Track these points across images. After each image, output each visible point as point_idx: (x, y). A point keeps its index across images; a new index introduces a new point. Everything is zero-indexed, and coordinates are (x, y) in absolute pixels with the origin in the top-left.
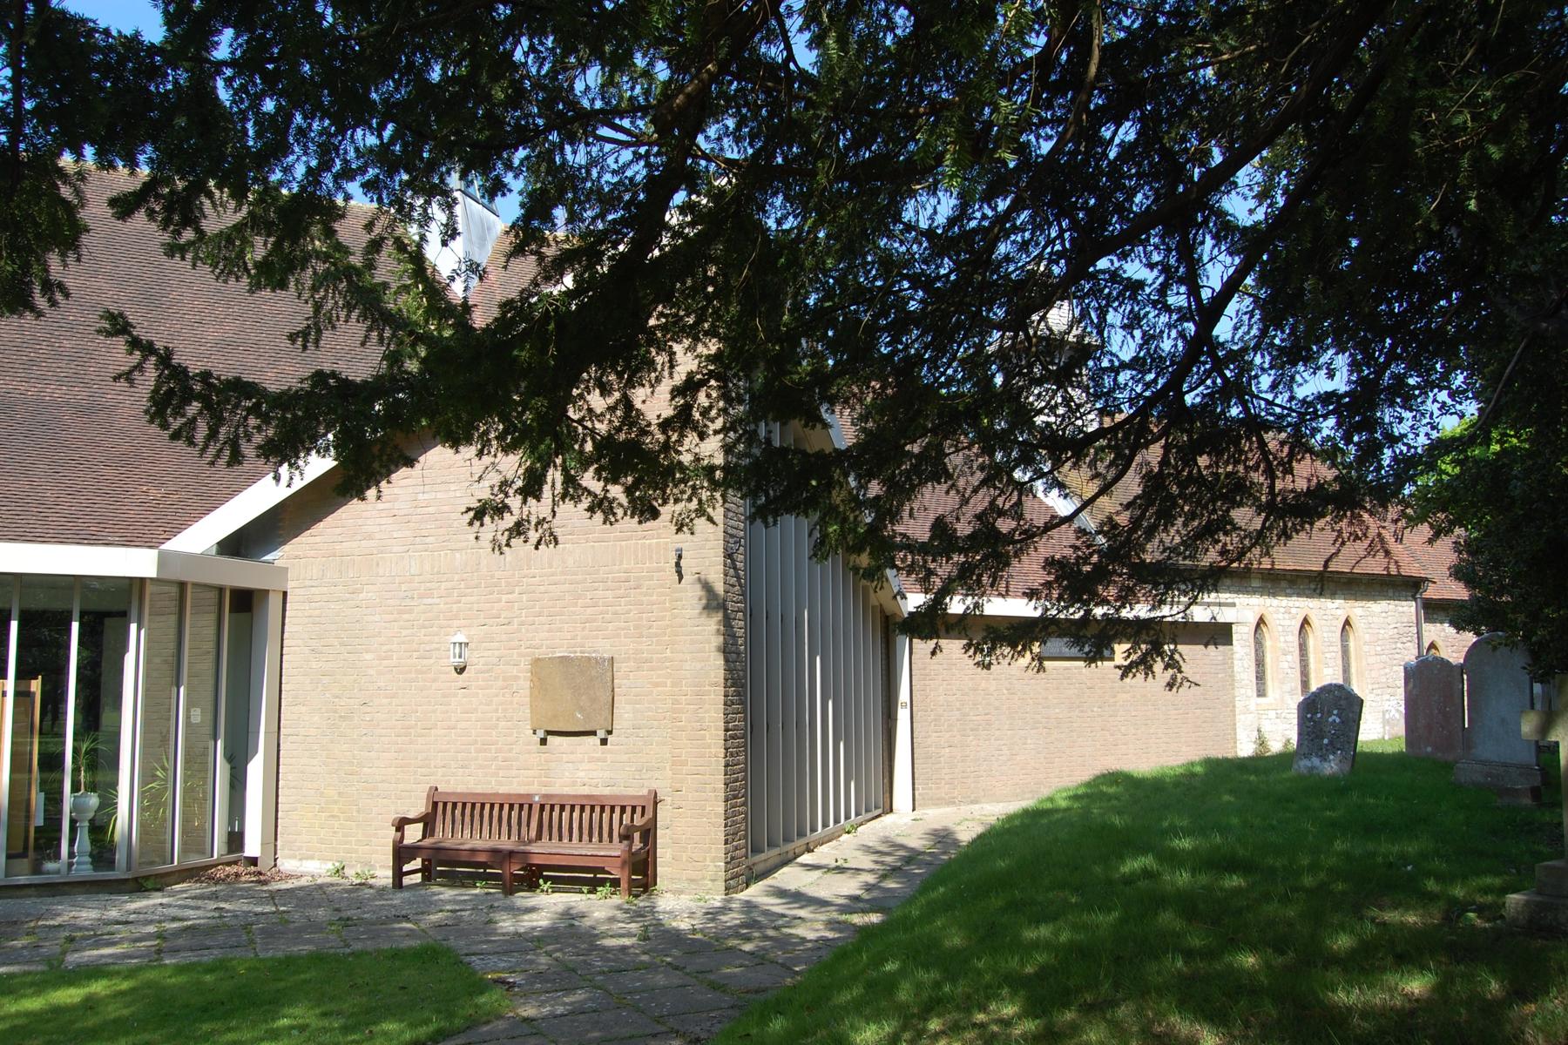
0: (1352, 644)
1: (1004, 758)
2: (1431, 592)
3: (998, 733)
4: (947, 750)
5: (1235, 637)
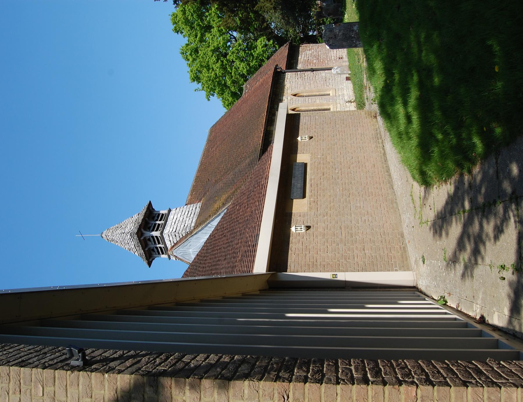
0: (305, 94)
2: (283, 66)
3: (353, 222)
4: (367, 252)
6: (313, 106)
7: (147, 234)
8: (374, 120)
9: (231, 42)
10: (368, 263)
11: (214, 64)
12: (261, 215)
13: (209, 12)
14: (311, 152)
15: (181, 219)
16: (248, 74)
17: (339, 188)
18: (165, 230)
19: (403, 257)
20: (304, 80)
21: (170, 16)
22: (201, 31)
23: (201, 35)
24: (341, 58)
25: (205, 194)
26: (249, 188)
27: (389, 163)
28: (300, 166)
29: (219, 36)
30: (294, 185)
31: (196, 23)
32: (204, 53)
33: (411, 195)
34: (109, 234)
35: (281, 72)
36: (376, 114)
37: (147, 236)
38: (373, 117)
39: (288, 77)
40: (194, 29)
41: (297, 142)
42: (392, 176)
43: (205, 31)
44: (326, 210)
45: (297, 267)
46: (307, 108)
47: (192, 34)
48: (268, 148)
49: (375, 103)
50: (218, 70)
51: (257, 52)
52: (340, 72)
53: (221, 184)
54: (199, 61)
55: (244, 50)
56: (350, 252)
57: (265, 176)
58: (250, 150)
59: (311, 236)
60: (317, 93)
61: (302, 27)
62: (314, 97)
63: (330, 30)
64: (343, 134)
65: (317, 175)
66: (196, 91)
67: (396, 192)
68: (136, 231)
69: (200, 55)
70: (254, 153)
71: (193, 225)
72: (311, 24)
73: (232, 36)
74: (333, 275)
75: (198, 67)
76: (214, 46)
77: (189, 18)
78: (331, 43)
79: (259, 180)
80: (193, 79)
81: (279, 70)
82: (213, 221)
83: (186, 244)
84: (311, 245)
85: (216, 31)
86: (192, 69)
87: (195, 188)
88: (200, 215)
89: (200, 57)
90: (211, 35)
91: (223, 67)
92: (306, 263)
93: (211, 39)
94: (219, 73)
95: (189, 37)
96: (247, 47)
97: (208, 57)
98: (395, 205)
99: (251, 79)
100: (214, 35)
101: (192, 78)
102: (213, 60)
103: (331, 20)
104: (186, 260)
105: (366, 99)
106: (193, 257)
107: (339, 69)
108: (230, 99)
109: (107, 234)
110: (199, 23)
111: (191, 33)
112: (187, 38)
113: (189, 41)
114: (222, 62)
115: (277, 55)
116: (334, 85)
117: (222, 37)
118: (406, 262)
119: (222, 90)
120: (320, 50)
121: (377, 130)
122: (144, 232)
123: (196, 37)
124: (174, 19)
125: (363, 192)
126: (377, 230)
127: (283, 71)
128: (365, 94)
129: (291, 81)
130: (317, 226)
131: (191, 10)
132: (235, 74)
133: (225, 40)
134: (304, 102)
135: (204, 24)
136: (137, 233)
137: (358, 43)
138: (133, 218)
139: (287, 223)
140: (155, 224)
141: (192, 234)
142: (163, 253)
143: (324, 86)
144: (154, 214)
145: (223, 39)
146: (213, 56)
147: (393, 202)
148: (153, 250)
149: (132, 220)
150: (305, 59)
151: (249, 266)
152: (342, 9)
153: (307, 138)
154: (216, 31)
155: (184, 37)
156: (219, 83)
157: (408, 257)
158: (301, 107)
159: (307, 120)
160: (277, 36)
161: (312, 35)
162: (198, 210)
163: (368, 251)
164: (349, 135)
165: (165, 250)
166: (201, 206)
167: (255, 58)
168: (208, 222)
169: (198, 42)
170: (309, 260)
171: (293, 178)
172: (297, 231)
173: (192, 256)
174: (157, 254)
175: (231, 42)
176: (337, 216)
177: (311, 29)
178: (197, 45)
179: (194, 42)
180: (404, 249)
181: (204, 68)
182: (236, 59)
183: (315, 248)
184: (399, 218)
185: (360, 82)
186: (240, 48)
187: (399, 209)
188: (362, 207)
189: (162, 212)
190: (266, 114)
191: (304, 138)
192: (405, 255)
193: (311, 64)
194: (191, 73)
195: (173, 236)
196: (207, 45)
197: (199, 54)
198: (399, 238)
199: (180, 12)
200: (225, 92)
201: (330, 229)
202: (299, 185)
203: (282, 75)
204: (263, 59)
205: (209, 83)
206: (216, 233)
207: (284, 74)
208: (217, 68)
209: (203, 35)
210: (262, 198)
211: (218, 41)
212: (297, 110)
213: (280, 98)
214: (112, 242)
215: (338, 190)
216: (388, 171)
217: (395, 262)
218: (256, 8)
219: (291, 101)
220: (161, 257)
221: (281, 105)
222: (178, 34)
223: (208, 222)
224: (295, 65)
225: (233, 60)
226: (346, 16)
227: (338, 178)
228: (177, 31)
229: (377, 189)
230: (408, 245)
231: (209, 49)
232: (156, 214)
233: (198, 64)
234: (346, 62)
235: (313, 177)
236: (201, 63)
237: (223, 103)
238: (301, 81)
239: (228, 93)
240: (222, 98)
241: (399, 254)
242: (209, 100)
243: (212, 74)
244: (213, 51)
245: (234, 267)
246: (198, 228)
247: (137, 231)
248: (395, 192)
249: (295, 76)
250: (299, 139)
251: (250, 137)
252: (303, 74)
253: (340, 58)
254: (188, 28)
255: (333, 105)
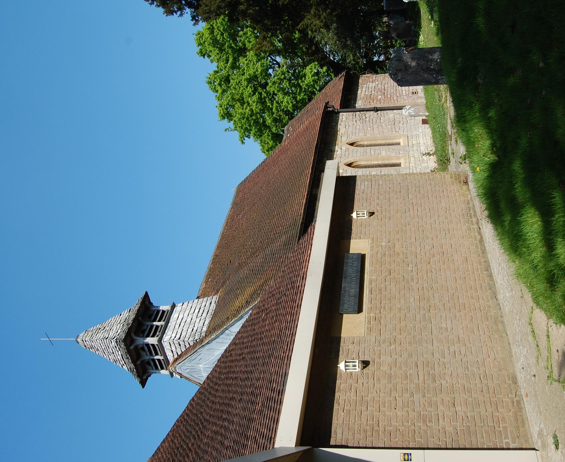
0: (366, 143)
2: (336, 103)
3: (437, 355)
4: (458, 408)
6: (377, 160)
7: (140, 341)
8: (465, 187)
9: (273, 68)
10: (461, 430)
11: (250, 97)
12: (293, 340)
13: (243, 31)
14: (371, 236)
15: (189, 319)
16: (294, 110)
18: (165, 335)
20: (364, 123)
22: (233, 55)
23: (233, 59)
24: (415, 93)
25: (224, 283)
26: (279, 288)
28: (354, 260)
29: (257, 62)
32: (237, 82)
33: (531, 324)
34: (86, 339)
37: (140, 344)
39: (343, 118)
41: (350, 220)
42: (494, 277)
44: (394, 334)
45: (347, 434)
46: (368, 163)
47: (221, 59)
50: (254, 104)
51: (306, 82)
52: (414, 114)
53: (245, 271)
54: (231, 93)
55: (290, 80)
56: (432, 409)
57: (301, 273)
59: (369, 378)
60: (383, 142)
62: (377, 147)
63: (398, 59)
65: (380, 274)
66: (226, 130)
68: (123, 337)
69: (232, 85)
70: (292, 228)
71: (205, 329)
74: (405, 454)
75: (229, 100)
77: (218, 38)
78: (399, 78)
79: (293, 278)
80: (222, 116)
82: (233, 327)
83: (194, 356)
84: (369, 395)
85: (253, 55)
86: (221, 103)
87: (211, 273)
88: (215, 315)
89: (231, 88)
91: (261, 101)
92: (362, 427)
93: (247, 65)
94: (256, 108)
95: (218, 62)
96: (293, 75)
97: (242, 88)
98: (500, 325)
99: (299, 115)
100: (250, 60)
101: (221, 114)
102: (248, 91)
104: (195, 380)
105: (452, 153)
106: (205, 375)
107: (412, 109)
108: (271, 143)
109: (84, 339)
110: (232, 44)
111: (220, 57)
112: (215, 64)
113: (218, 68)
116: (406, 131)
117: (260, 62)
119: (260, 130)
121: (468, 203)
122: (136, 338)
123: (227, 63)
125: (450, 304)
126: (475, 370)
127: (336, 110)
128: (450, 146)
129: (346, 124)
130: (379, 360)
131: (221, 28)
132: (276, 110)
133: (264, 66)
135: (237, 46)
136: (125, 341)
137: (440, 78)
138: (121, 316)
140: (152, 326)
141: (203, 344)
144: (152, 310)
145: (261, 65)
146: (249, 87)
147: (499, 320)
148: (148, 363)
149: (120, 319)
150: (367, 93)
151: (271, 428)
152: (415, 28)
153: (365, 215)
154: (253, 55)
156: (256, 122)
157: (526, 420)
158: (359, 161)
160: (333, 62)
161: (378, 61)
162: (213, 306)
163: (460, 408)
164: (427, 210)
165: (164, 364)
166: (218, 301)
167: (303, 90)
168: (225, 327)
169: (229, 69)
170: (365, 423)
171: (344, 278)
173: (203, 374)
174: (154, 369)
175: (273, 69)
177: (376, 53)
179: (225, 69)
180: (518, 405)
182: (278, 91)
183: (376, 401)
187: (508, 333)
188: (449, 330)
190: (310, 172)
192: (521, 416)
193: (375, 101)
195: (176, 345)
197: (231, 84)
198: (509, 385)
199: (207, 31)
200: (264, 134)
202: (353, 290)
203: (335, 115)
204: (313, 91)
205: (243, 121)
207: (338, 115)
209: (236, 60)
210: (295, 310)
211: (255, 68)
212: (354, 165)
213: (331, 148)
214: (91, 350)
215: (412, 300)
216: (488, 268)
217: (505, 428)
218: (299, 26)
219: (347, 152)
222: (204, 58)
223: (225, 327)
224: (352, 102)
225: (274, 92)
226: (421, 38)
227: (412, 279)
230: (525, 400)
231: (244, 77)
232: (154, 311)
233: (229, 97)
234: (421, 98)
235: (373, 278)
236: (232, 96)
237: (261, 148)
239: (268, 135)
240: (260, 141)
241: (511, 414)
242: (243, 143)
243: (247, 110)
244: (249, 81)
245: (251, 420)
246: (211, 336)
247: (125, 337)
248: (499, 304)
249: (353, 118)
250: (354, 215)
251: (288, 203)
252: (363, 115)
253: (413, 93)
254: (217, 51)
255: (405, 159)
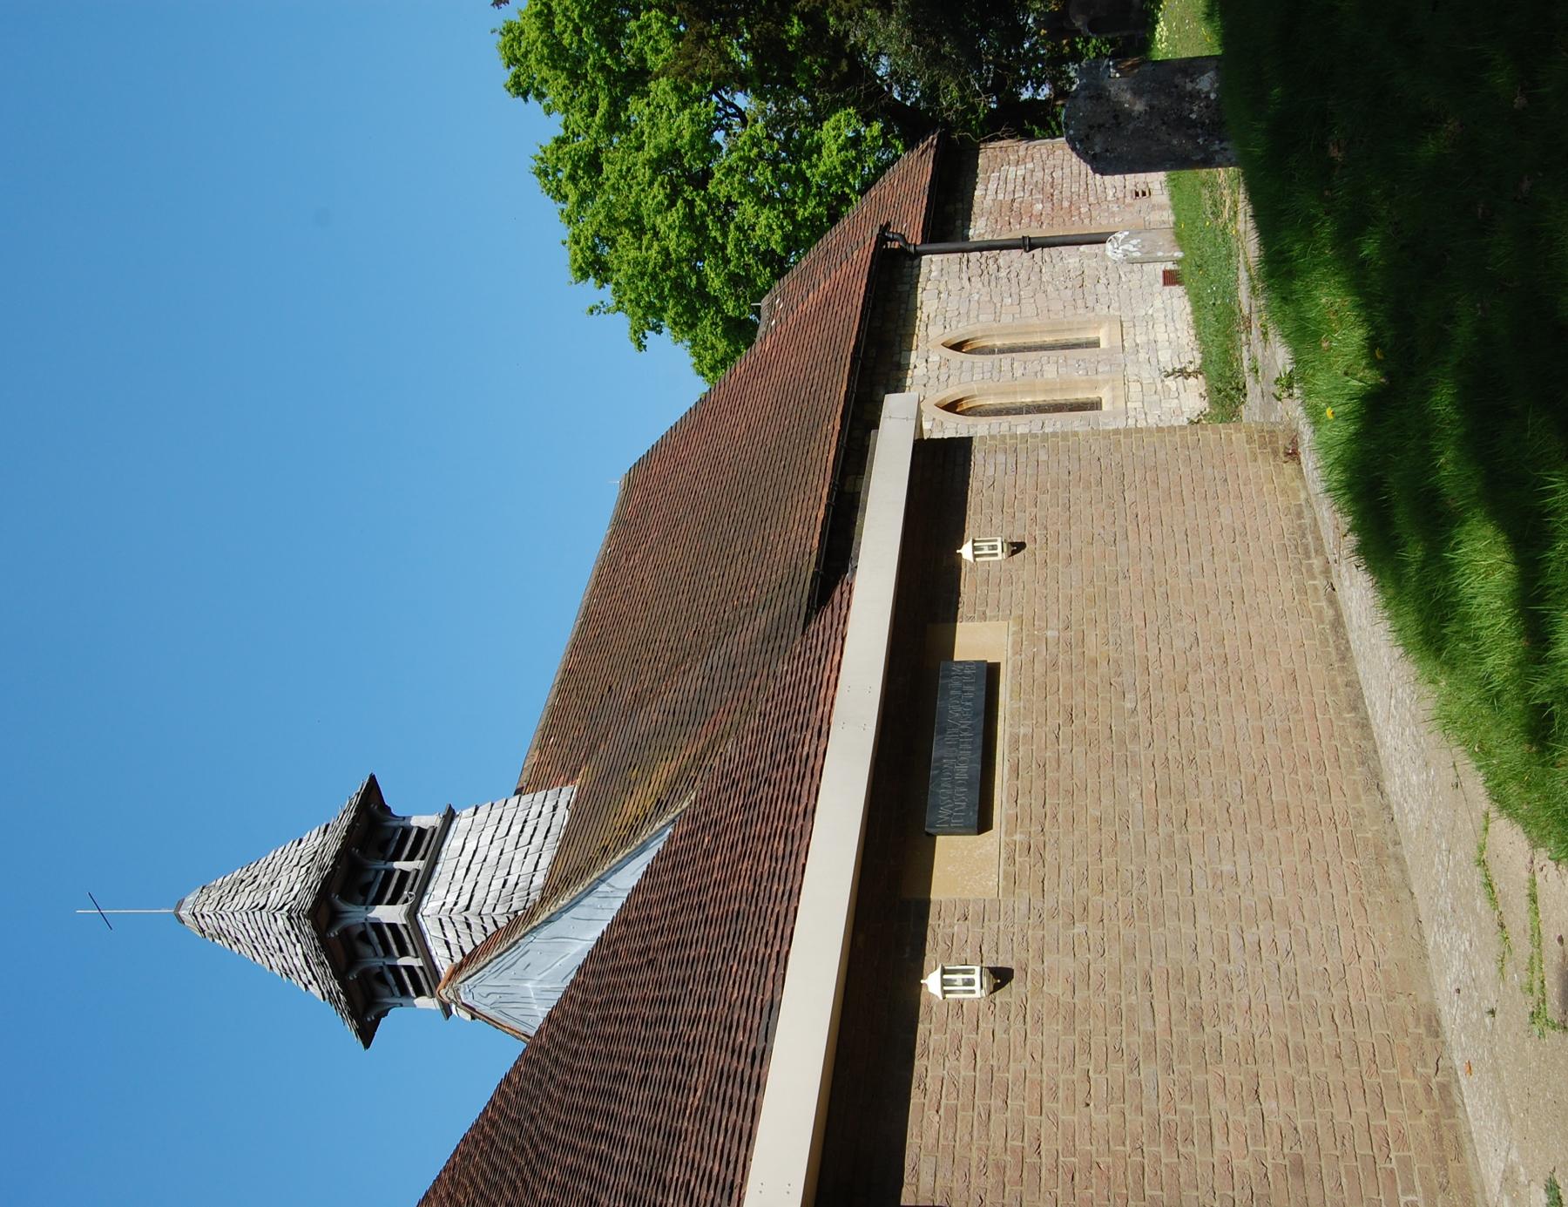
0: (998, 343)
1: (1282, 935)
2: (911, 227)
3: (1206, 953)
4: (1269, 1105)
5: (1005, 965)
6: (1032, 392)
7: (357, 915)
8: (1289, 468)
10: (1276, 1166)
11: (659, 212)
12: (792, 909)
13: (638, 19)
14: (1016, 612)
15: (495, 853)
16: (788, 250)
17: (1139, 784)
19: (1441, 1137)
20: (993, 284)
21: (497, 34)
22: (609, 90)
23: (610, 104)
24: (1144, 194)
25: (593, 748)
26: (751, 762)
27: (1361, 667)
28: (966, 679)
29: (678, 110)
30: (940, 769)
31: (590, 61)
32: (621, 171)
33: (1482, 863)
34: (205, 911)
35: (902, 252)
36: (1294, 442)
38: (1282, 455)
39: (930, 271)
40: (587, 82)
41: (955, 566)
42: (1375, 728)
43: (628, 92)
46: (1006, 401)
48: (835, 586)
49: (1291, 395)
50: (673, 235)
51: (822, 168)
52: (1139, 254)
53: (651, 715)
54: (604, 203)
55: (774, 162)
56: (1193, 1107)
57: (815, 719)
58: (774, 576)
59: (1012, 1018)
60: (1049, 339)
61: (995, 73)
64: (1156, 531)
66: (591, 311)
67: (1395, 808)
69: (608, 179)
70: (787, 590)
71: (539, 880)
72: (1030, 59)
73: (732, 105)
75: (601, 224)
76: (658, 148)
77: (566, 42)
78: (1098, 149)
81: (896, 245)
83: (509, 958)
85: (667, 89)
86: (577, 231)
88: (568, 839)
89: (606, 187)
90: (648, 105)
91: (693, 224)
92: (991, 1157)
93: (649, 120)
94: (678, 246)
95: (567, 111)
96: (784, 146)
97: (636, 189)
98: (1392, 871)
99: (803, 263)
100: (658, 106)
101: (577, 265)
102: (655, 197)
103: (1104, 44)
104: (512, 1024)
105: (1251, 370)
106: (540, 1011)
107: (1134, 242)
108: (722, 346)
110: (605, 58)
111: (573, 97)
113: (567, 128)
114: (690, 204)
115: (891, 185)
116: (1115, 305)
117: (688, 111)
118: (1455, 1164)
119: (691, 310)
120: (1060, 162)
121: (1300, 515)
122: (344, 906)
123: (593, 114)
124: (512, 46)
125: (1245, 807)
126: (1317, 995)
127: (912, 248)
128: (1245, 348)
129: (942, 288)
130: (1039, 967)
131: (573, 11)
133: (699, 122)
134: (995, 373)
135: (619, 64)
136: (313, 914)
137: (1216, 147)
138: (303, 845)
139: (908, 949)
140: (390, 873)
141: (535, 923)
142: (420, 992)
143: (1075, 308)
145: (692, 120)
146: (656, 185)
148: (381, 978)
149: (298, 853)
150: (1001, 197)
151: (733, 1158)
154: (667, 89)
155: (548, 111)
159: (1001, 468)
161: (1033, 101)
162: (563, 815)
163: (1274, 1105)
164: (1179, 536)
165: (424, 980)
166: (577, 802)
167: (814, 190)
168: (596, 875)
169: (598, 133)
170: (1001, 1143)
171: (938, 734)
172: (949, 992)
173: (536, 1007)
174: (398, 993)
176: (1129, 918)
177: (1027, 78)
178: (595, 141)
179: (587, 132)
180: (1445, 1098)
181: (623, 229)
182: (742, 195)
184: (1416, 937)
185: (1223, 298)
186: (755, 150)
187: (1414, 890)
188: (1243, 880)
189: (417, 821)
190: (838, 428)
191: (986, 551)
192: (1452, 1127)
193: (1025, 220)
194: (576, 247)
195: (458, 927)
196: (634, 143)
198: (1419, 1040)
199: (533, 20)
200: (701, 319)
201: (1102, 987)
202: (963, 767)
203: (908, 263)
204: (843, 192)
205: (640, 284)
206: (620, 939)
207: (916, 262)
208: (670, 227)
209: (617, 105)
210: (799, 825)
212: (965, 407)
213: (896, 358)
214: (217, 941)
215: (1134, 794)
216: (1356, 702)
217: (1405, 1163)
220: (415, 1006)
221: (892, 402)
222: (526, 100)
223: (596, 875)
224: (959, 223)
225: (729, 197)
226: (1161, 30)
227: (1136, 735)
228: (522, 89)
229: (1311, 789)
230: (1463, 1081)
231: (642, 157)
232: (395, 829)
233: (598, 213)
234: (1161, 208)
235: (1022, 731)
236: (609, 211)
237: (694, 360)
238: (985, 290)
242: (641, 346)
243: (653, 253)
244: (657, 166)
245: (674, 1136)
246: (557, 900)
248: (1389, 807)
249: (961, 270)
250: (966, 551)
252: (991, 262)
253: (1137, 194)
254: (563, 80)
255: (1113, 389)
